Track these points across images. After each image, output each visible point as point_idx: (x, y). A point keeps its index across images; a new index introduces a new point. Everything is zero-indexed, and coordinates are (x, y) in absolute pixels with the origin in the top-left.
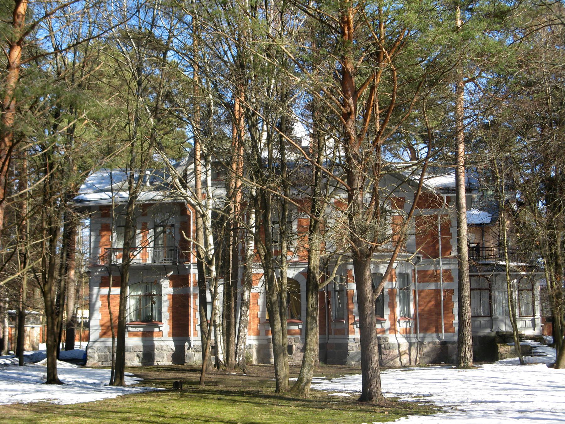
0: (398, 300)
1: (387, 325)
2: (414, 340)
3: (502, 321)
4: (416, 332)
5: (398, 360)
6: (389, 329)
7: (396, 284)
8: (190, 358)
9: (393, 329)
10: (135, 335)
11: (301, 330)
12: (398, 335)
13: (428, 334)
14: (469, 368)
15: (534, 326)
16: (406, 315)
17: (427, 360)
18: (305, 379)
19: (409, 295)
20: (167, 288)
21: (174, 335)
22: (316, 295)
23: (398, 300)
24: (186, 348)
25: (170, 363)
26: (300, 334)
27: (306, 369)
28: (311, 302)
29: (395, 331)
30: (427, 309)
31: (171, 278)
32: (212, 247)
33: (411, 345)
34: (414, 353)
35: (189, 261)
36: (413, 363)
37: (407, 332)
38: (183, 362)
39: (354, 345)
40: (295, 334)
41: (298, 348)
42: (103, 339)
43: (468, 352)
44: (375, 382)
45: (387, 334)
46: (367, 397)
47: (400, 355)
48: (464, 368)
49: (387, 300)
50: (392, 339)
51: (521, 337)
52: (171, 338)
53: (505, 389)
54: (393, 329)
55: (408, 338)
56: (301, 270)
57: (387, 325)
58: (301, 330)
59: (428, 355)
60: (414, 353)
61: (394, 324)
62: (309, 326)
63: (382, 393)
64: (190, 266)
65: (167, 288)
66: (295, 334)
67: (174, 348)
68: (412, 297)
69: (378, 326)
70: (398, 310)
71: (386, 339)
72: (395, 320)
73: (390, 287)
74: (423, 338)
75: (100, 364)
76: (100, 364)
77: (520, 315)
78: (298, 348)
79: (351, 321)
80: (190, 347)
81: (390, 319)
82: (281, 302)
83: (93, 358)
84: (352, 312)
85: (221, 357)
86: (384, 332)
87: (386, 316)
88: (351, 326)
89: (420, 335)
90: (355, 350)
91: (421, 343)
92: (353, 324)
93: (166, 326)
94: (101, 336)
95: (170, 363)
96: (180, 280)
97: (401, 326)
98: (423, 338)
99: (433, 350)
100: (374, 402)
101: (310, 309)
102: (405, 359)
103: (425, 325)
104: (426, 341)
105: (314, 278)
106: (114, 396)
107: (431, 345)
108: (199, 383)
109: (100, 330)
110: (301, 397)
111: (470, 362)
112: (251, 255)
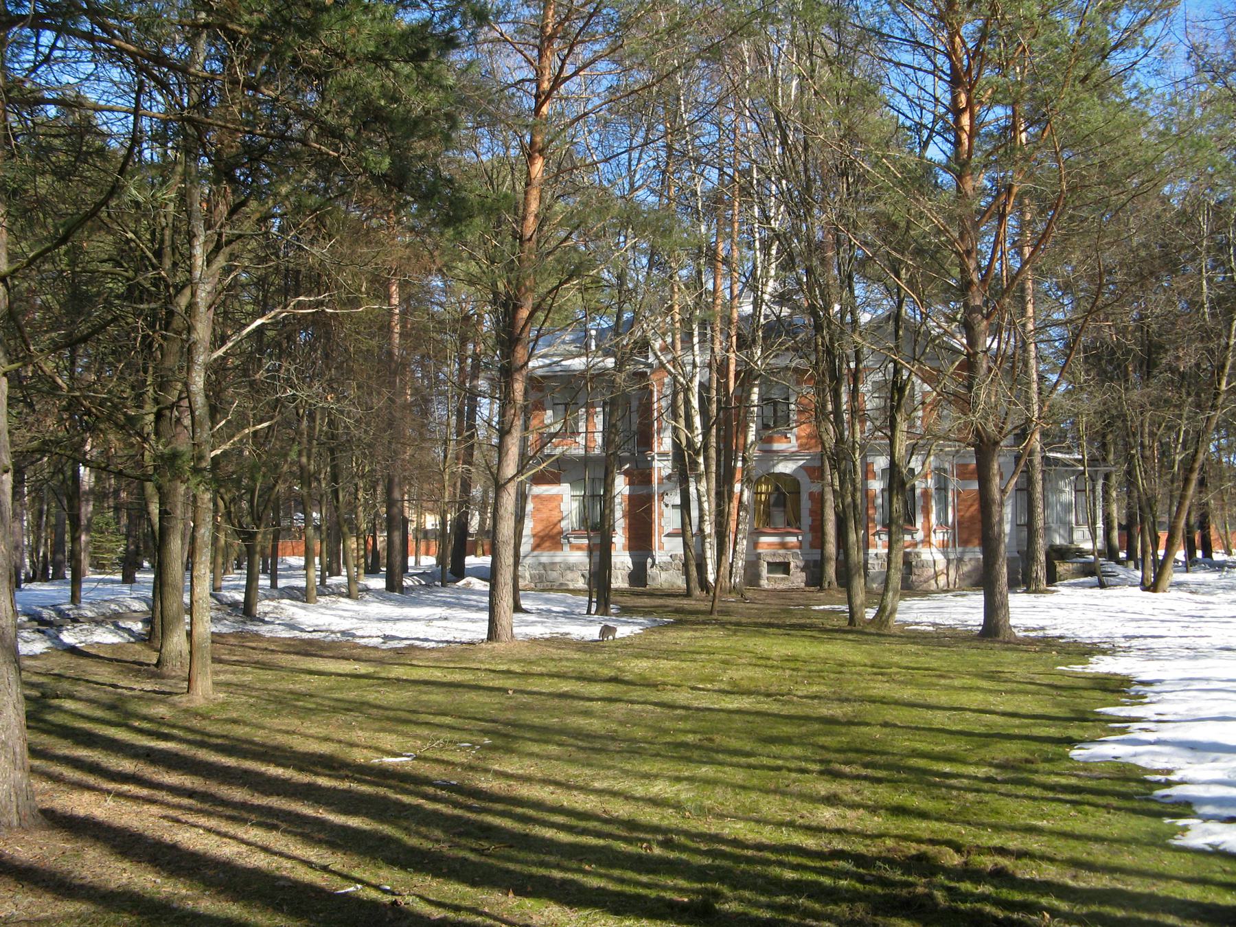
0: (933, 503)
1: (919, 536)
2: (952, 556)
3: (1056, 531)
4: (954, 546)
5: (933, 582)
6: (922, 542)
7: (931, 482)
8: (654, 579)
9: (927, 542)
10: (579, 548)
11: (800, 542)
12: (934, 550)
13: (970, 547)
14: (1042, 592)
15: (1094, 539)
16: (943, 523)
17: (968, 582)
18: (889, 608)
19: (946, 497)
20: (621, 486)
21: (630, 549)
22: (903, 495)
23: (933, 503)
24: (649, 566)
25: (626, 585)
26: (800, 548)
27: (890, 594)
28: (895, 506)
29: (930, 544)
30: (968, 514)
31: (626, 473)
32: (700, 431)
33: (949, 562)
34: (952, 573)
35: (652, 450)
36: (951, 586)
37: (944, 546)
38: (1013, 585)
39: (876, 562)
40: (792, 548)
41: (797, 567)
42: (535, 553)
43: (1040, 571)
44: (1002, 613)
45: (920, 549)
46: (993, 628)
47: (936, 575)
48: (1035, 592)
49: (919, 503)
50: (926, 554)
51: (1081, 553)
52: (627, 553)
53: (1133, 620)
54: (927, 542)
55: (945, 554)
56: (801, 462)
57: (919, 536)
58: (800, 542)
59: (968, 575)
60: (952, 573)
61: (928, 535)
62: (894, 538)
63: (1010, 627)
64: (653, 458)
65: (621, 486)
66: (792, 548)
67: (631, 566)
68: (950, 499)
69: (907, 538)
70: (933, 517)
71: (918, 555)
72: (929, 530)
73: (923, 486)
74: (963, 553)
75: (533, 585)
76: (533, 585)
77: (1077, 523)
78: (797, 567)
79: (871, 532)
80: (654, 564)
81: (923, 528)
82: (855, 507)
83: (524, 578)
84: (873, 520)
85: (711, 578)
86: (915, 545)
87: (919, 525)
88: (871, 538)
89: (959, 549)
90: (877, 569)
91: (960, 560)
92: (874, 535)
93: (620, 539)
94: (533, 549)
95: (626, 585)
96: (641, 477)
97: (938, 537)
98: (963, 553)
99: (975, 570)
100: (1001, 638)
101: (895, 515)
102: (942, 580)
103: (965, 536)
104: (966, 558)
105: (900, 472)
106: (637, 629)
107: (973, 563)
108: (711, 613)
109: (532, 541)
110: (886, 632)
111: (1043, 585)
112: (752, 443)
